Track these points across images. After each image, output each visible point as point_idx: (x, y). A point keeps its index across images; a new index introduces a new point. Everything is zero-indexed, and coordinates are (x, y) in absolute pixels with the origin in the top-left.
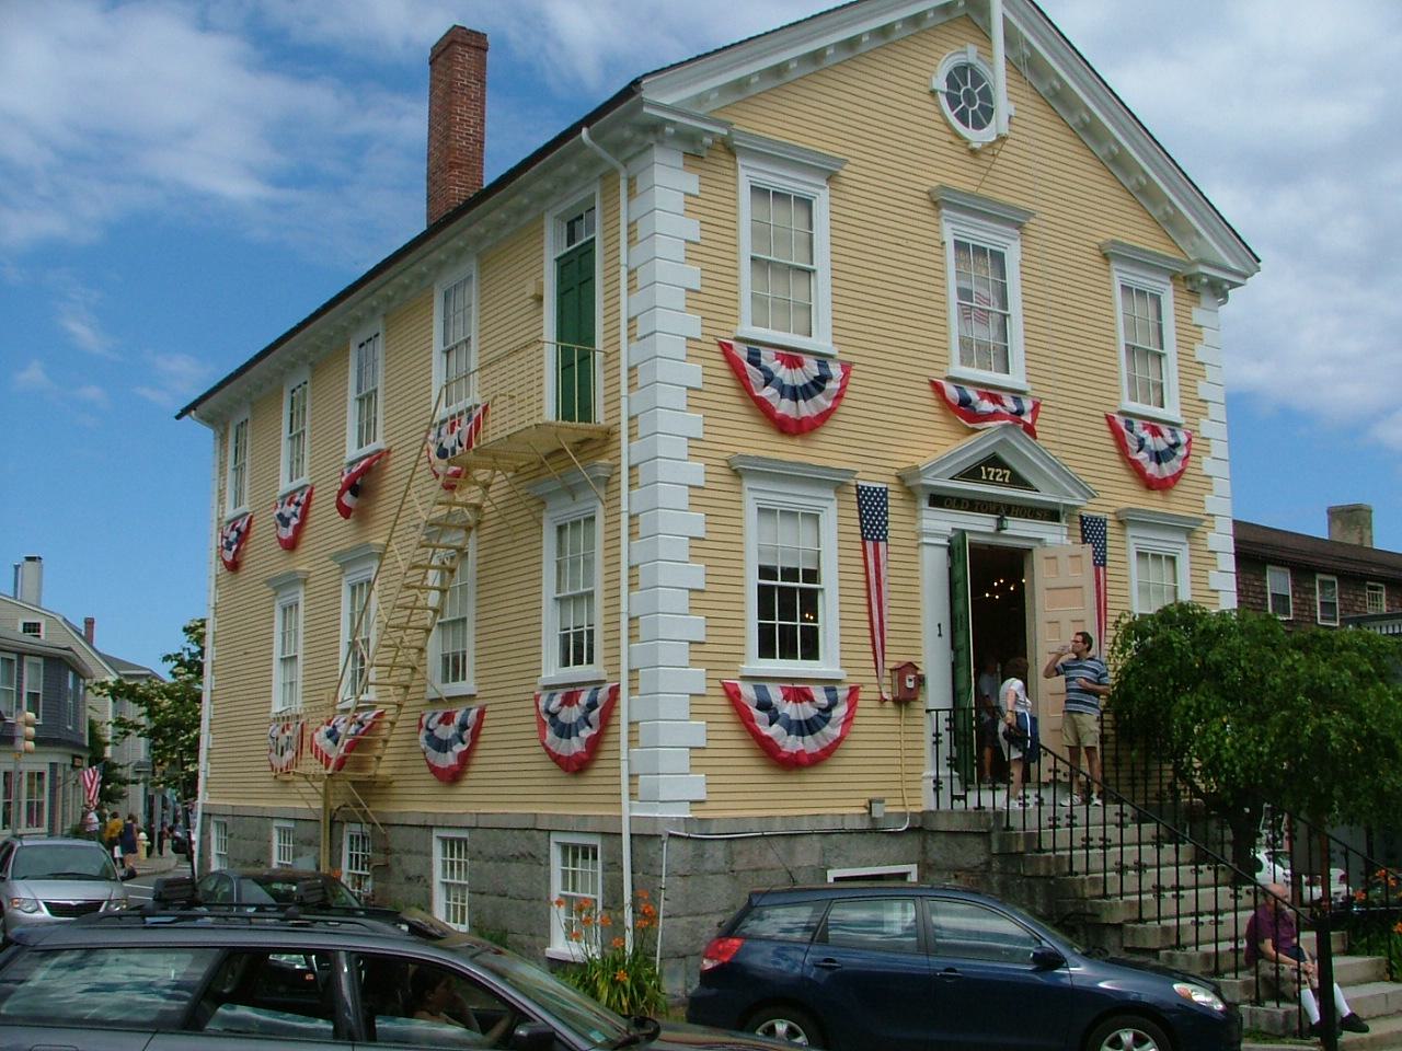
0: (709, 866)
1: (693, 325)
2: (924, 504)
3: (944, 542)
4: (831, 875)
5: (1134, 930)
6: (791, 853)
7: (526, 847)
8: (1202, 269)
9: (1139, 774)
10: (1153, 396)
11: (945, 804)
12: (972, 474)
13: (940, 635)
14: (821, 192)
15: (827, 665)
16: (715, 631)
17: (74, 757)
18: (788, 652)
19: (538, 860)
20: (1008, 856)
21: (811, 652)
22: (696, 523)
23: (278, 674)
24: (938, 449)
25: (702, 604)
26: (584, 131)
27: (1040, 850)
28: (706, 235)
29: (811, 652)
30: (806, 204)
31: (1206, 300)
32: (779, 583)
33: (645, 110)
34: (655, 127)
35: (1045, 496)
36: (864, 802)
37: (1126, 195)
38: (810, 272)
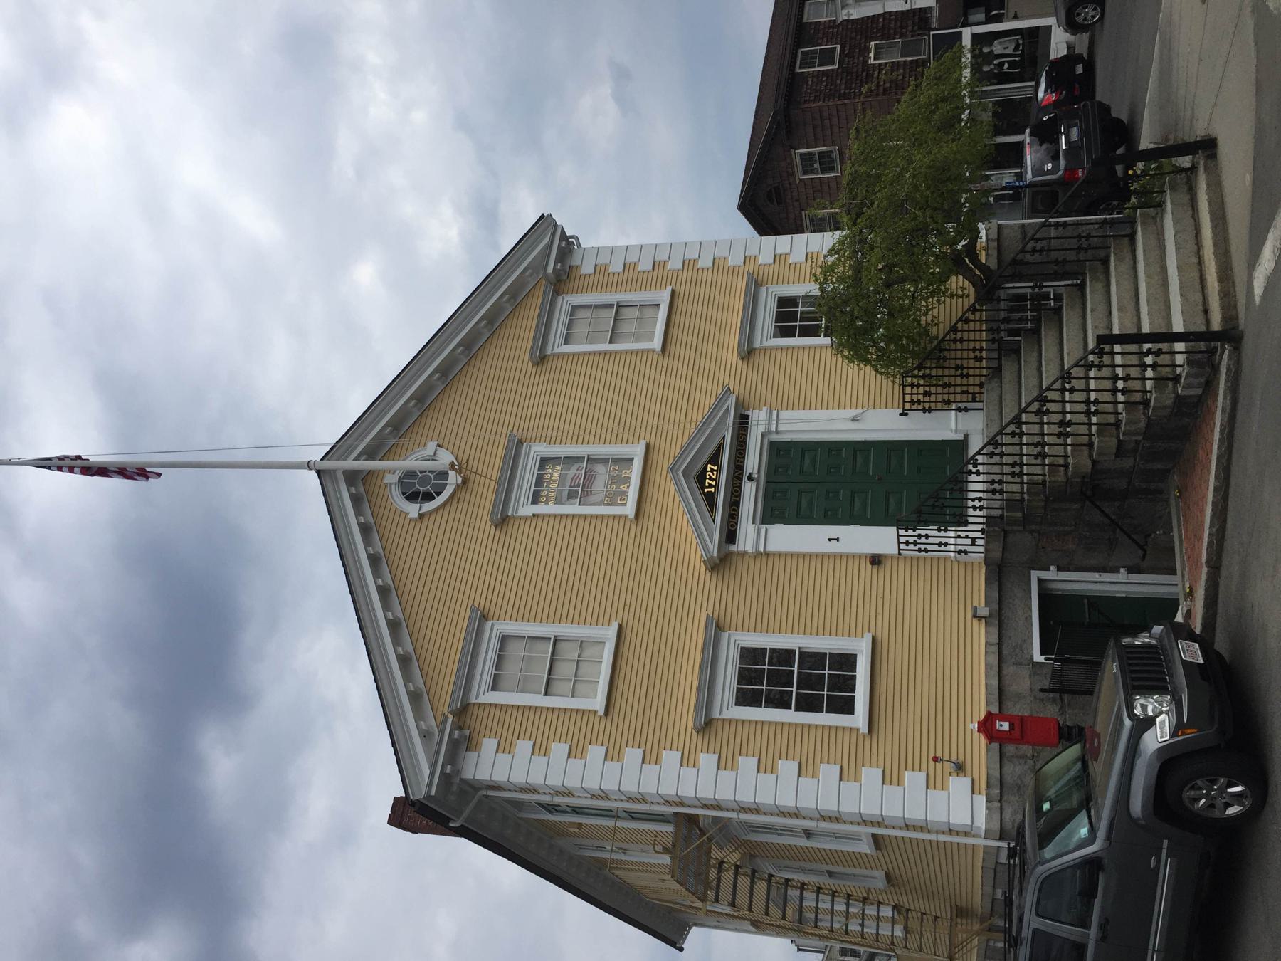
2: (733, 548)
4: (1039, 658)
5: (1099, 454)
8: (550, 270)
9: (959, 372)
10: (649, 312)
12: (710, 499)
13: (837, 539)
14: (496, 628)
16: (832, 756)
20: (1026, 520)
21: (848, 661)
22: (747, 764)
25: (810, 768)
29: (848, 661)
30: (504, 640)
31: (576, 260)
32: (794, 690)
33: (433, 793)
34: (446, 779)
36: (975, 622)
37: (496, 336)
38: (556, 640)
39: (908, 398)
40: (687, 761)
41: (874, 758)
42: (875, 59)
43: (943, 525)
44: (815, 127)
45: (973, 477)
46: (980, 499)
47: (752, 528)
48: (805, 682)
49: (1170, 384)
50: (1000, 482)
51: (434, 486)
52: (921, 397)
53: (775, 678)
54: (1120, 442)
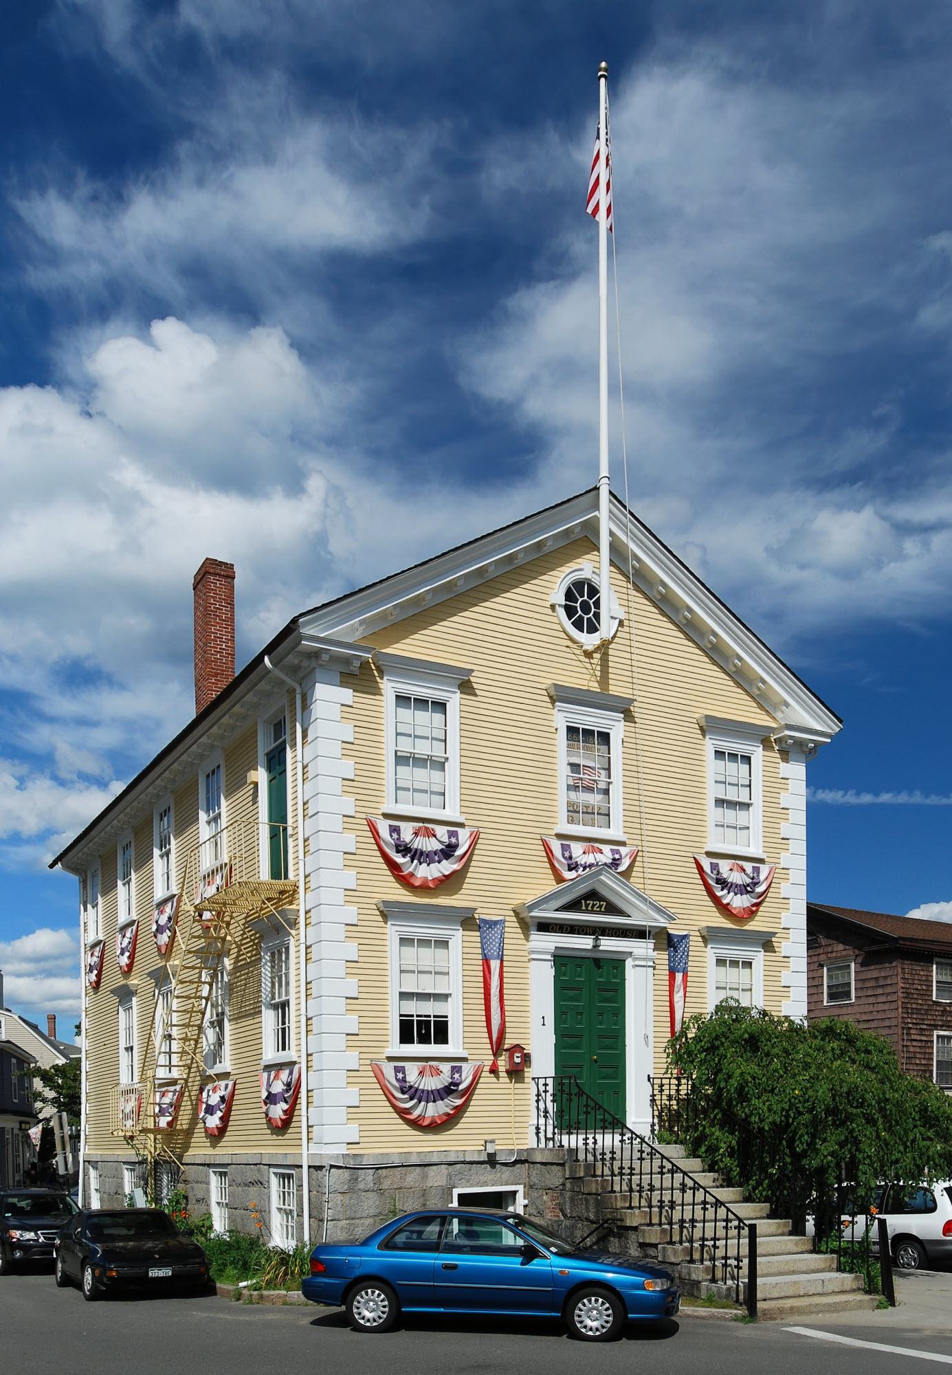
0: (361, 1186)
1: (348, 805)
3: (549, 957)
4: (456, 1192)
5: (644, 1231)
6: (425, 1177)
7: (256, 1177)
11: (542, 1145)
12: (573, 906)
15: (452, 1048)
17: (21, 1123)
18: (424, 1039)
19: (262, 1184)
20: (575, 1179)
22: (351, 950)
23: (124, 1057)
24: (537, 886)
26: (266, 659)
27: (595, 1176)
28: (357, 736)
34: (315, 654)
35: (635, 920)
39: (665, 1081)
42: (938, 1036)
43: (560, 1114)
44: (877, 979)
45: (618, 1137)
46: (595, 1143)
47: (551, 947)
49: (710, 1277)
50: (613, 1159)
51: (581, 618)
52: (667, 1092)
54: (655, 1246)
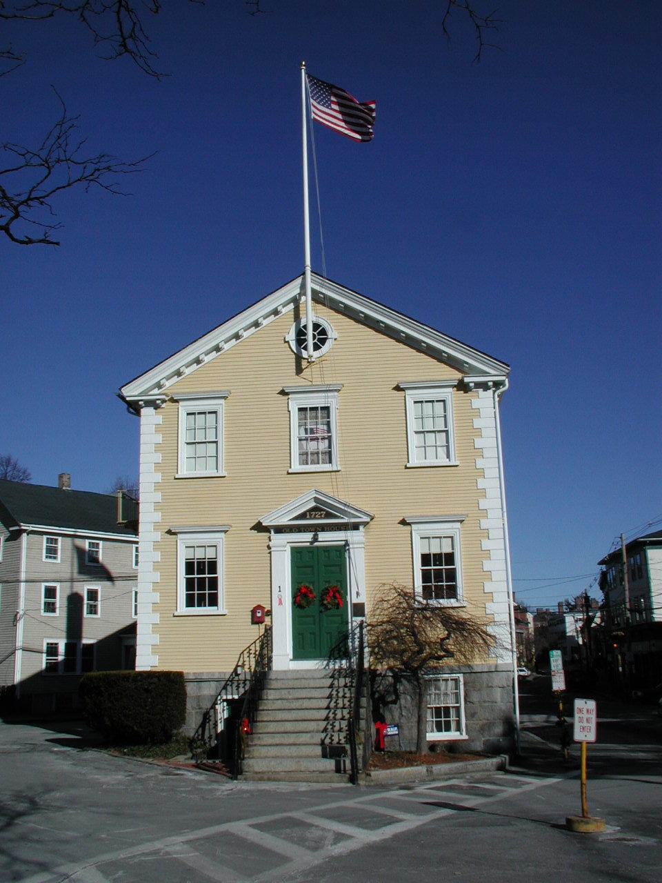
32: (196, 576)
40: (157, 526)
41: (167, 420)
48: (201, 581)
53: (202, 587)
